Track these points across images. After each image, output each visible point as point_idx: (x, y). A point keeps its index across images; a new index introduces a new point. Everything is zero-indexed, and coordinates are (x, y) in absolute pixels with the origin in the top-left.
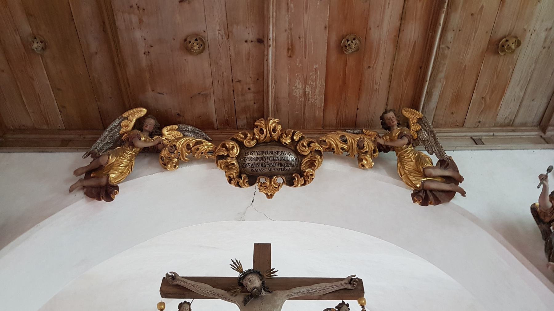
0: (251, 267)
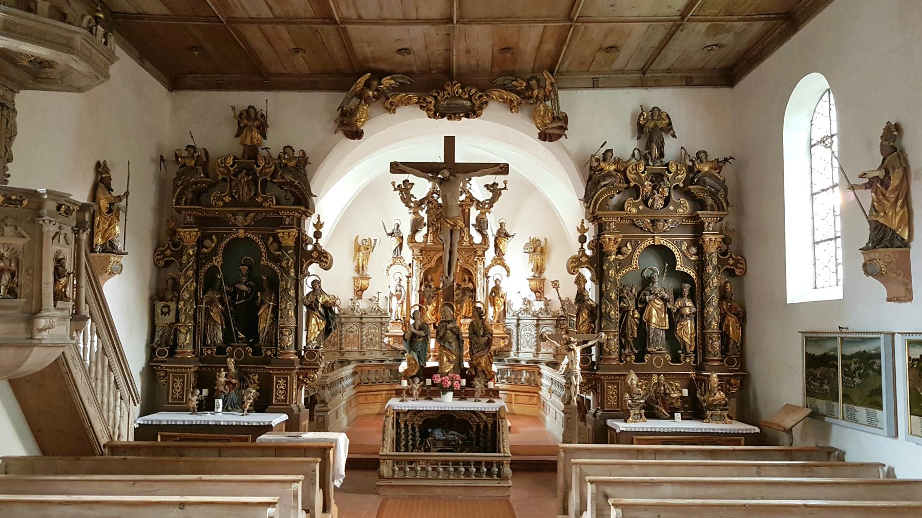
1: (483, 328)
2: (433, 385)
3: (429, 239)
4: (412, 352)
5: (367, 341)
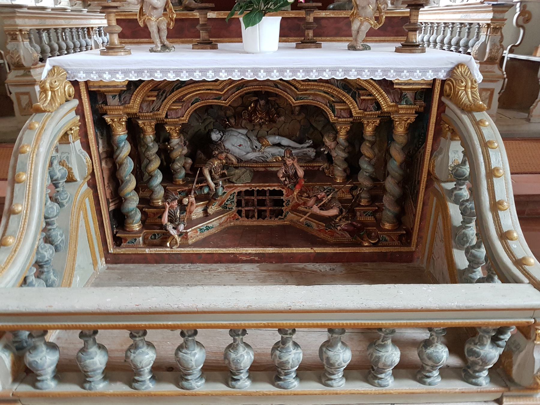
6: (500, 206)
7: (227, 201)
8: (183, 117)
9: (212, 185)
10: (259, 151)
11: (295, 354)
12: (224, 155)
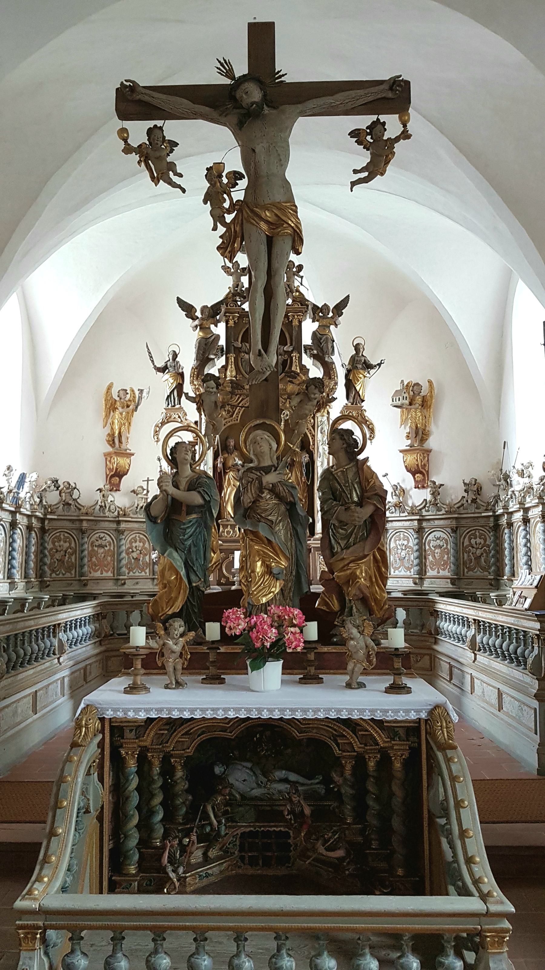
0: (246, 72)
1: (360, 483)
2: (226, 639)
3: (228, 373)
4: (170, 550)
5: (130, 562)
6: (466, 834)
7: (229, 844)
8: (189, 749)
9: (215, 822)
10: (265, 787)
11: (288, 961)
12: (227, 791)
